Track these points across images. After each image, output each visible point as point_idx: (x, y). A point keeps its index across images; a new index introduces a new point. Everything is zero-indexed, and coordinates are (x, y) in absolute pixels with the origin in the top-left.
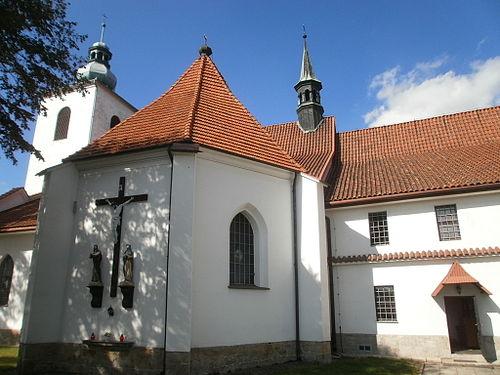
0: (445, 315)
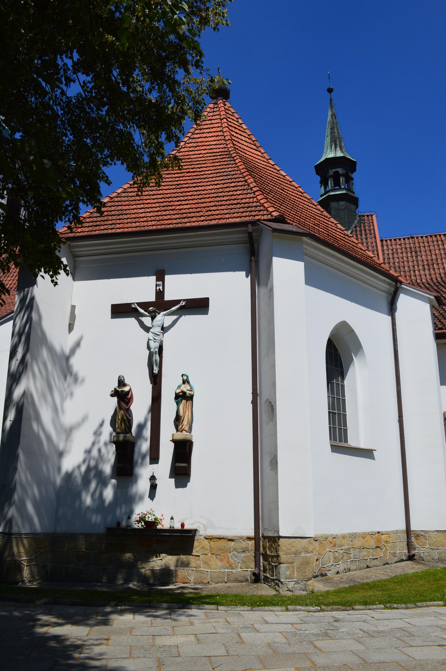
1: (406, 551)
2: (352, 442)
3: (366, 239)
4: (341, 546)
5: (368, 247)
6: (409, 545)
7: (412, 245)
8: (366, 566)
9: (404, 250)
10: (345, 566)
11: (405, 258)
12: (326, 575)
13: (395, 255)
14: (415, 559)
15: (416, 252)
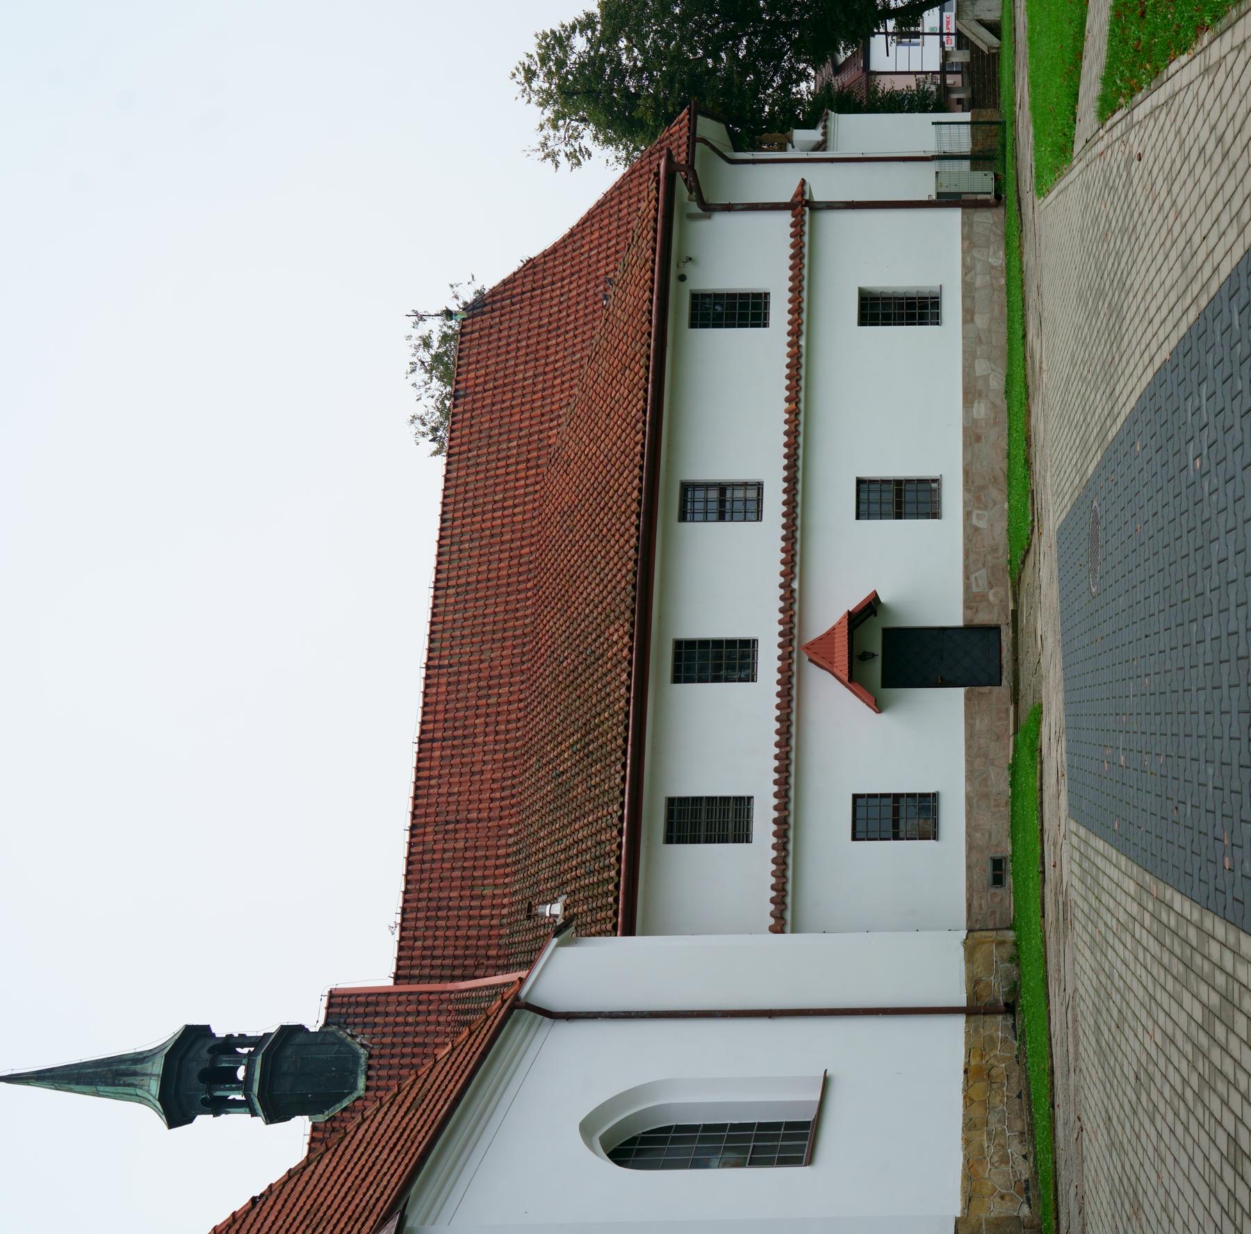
0: (297, 1117)
1: (1000, 1018)
2: (810, 1118)
3: (387, 1014)
4: (982, 1147)
5: (412, 1066)
6: (990, 1010)
7: (421, 915)
8: (1017, 1100)
9: (430, 933)
10: (1016, 1142)
11: (448, 933)
12: (1027, 1181)
13: (438, 952)
14: (1013, 1002)
15: (439, 909)
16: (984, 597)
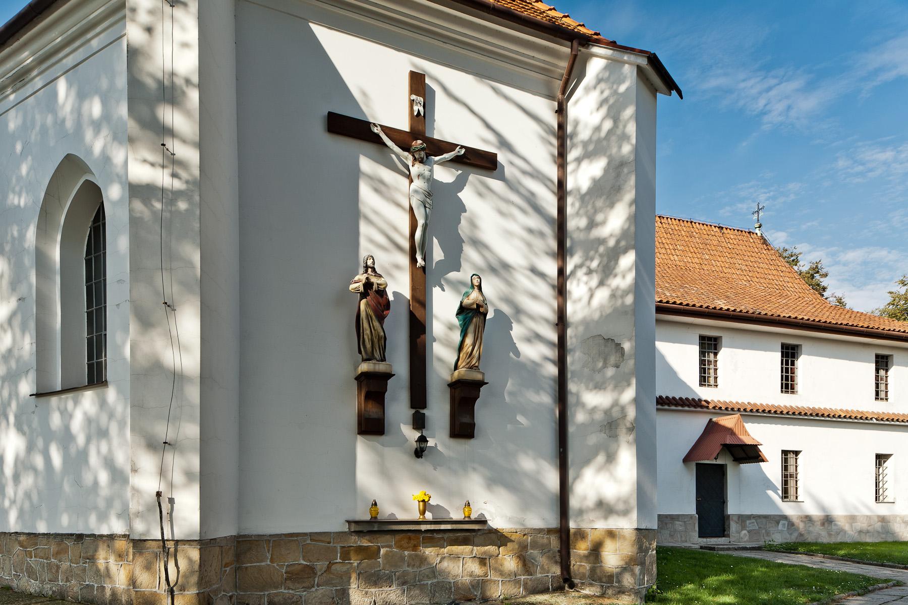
16: (743, 528)
